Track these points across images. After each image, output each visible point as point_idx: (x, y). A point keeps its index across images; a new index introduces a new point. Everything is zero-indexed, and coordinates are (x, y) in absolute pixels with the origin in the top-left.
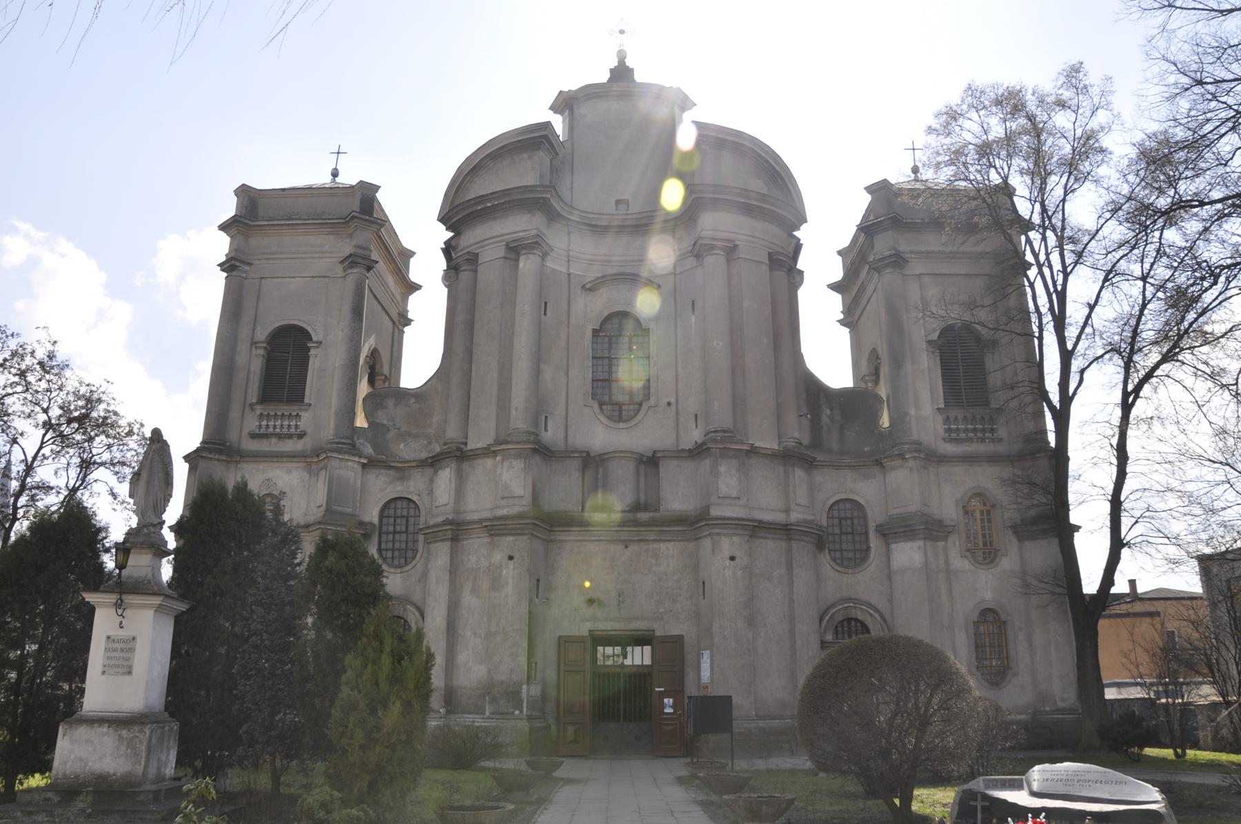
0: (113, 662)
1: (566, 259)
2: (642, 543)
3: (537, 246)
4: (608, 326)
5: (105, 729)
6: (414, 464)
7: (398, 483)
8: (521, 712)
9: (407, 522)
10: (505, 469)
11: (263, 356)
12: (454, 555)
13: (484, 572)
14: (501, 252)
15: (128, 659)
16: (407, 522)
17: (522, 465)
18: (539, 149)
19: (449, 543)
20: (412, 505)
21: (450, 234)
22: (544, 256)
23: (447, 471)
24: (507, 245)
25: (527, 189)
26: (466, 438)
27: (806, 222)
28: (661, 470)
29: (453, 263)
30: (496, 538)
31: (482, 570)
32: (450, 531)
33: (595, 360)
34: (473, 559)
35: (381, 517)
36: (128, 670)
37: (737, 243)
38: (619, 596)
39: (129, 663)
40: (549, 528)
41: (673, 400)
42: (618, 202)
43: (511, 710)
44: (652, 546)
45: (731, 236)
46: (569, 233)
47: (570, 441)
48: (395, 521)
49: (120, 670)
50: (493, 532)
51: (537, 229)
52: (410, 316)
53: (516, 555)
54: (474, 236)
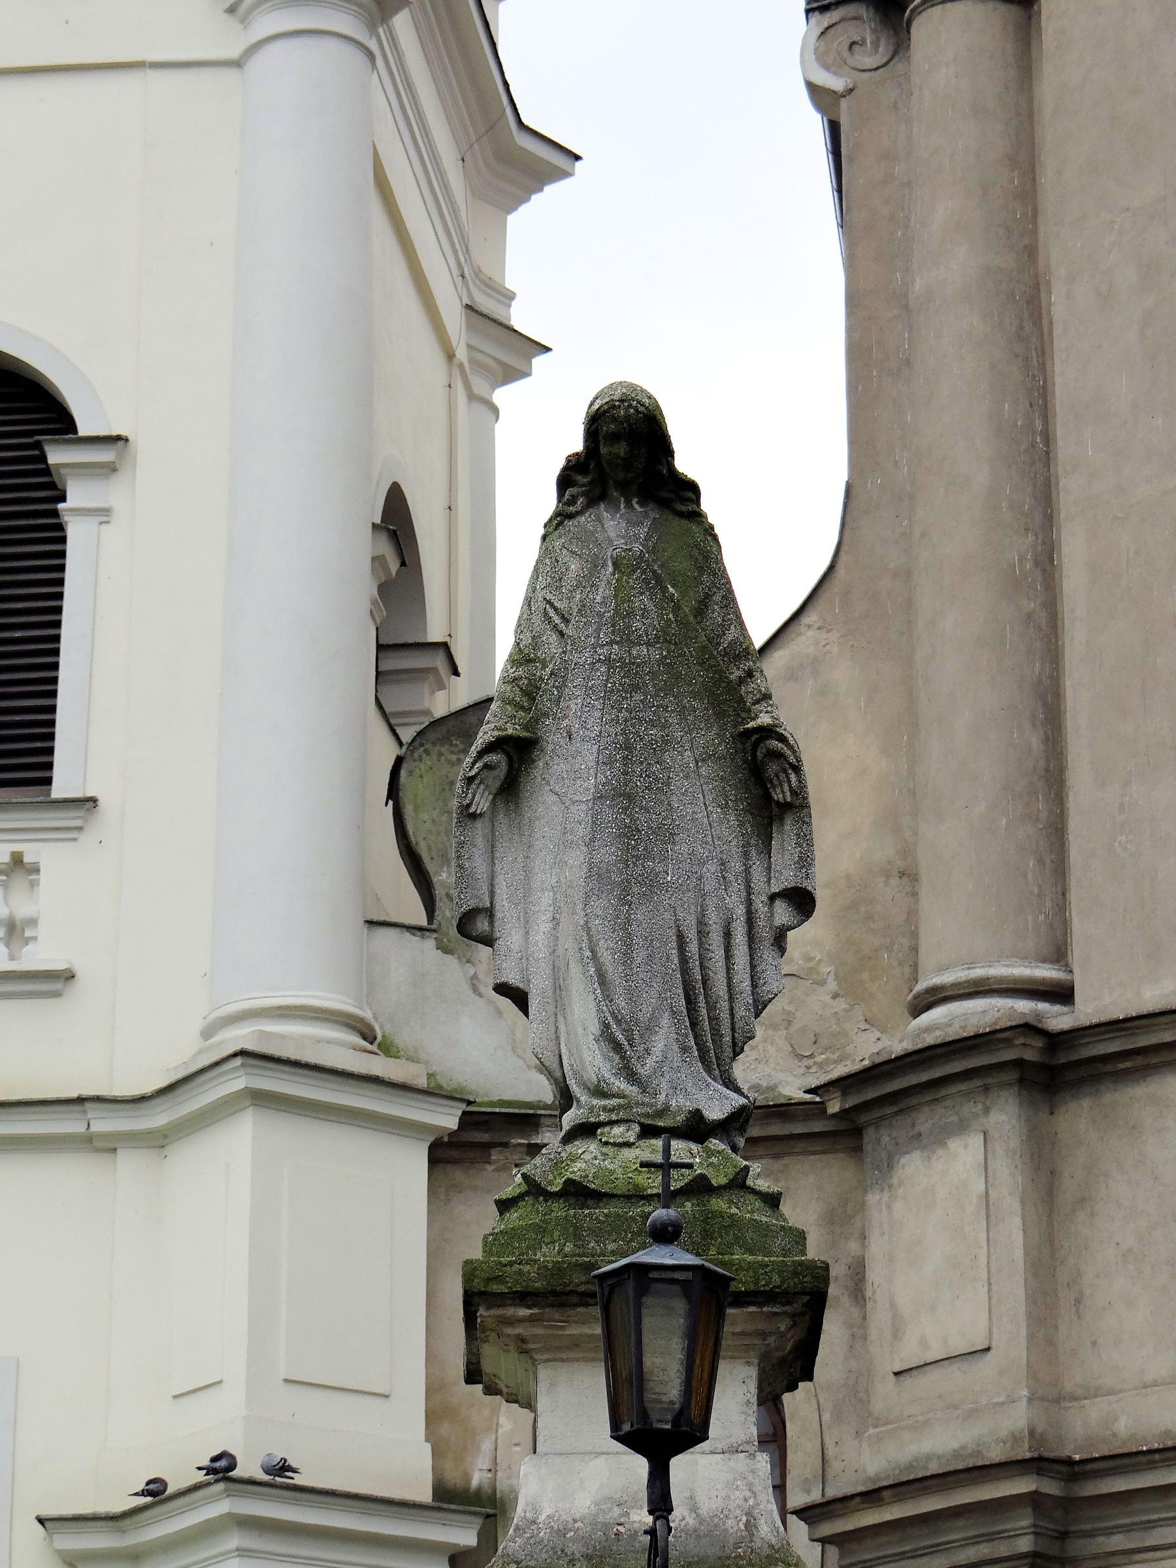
26: (1059, 954)
32: (1024, 1521)
52: (521, 319)
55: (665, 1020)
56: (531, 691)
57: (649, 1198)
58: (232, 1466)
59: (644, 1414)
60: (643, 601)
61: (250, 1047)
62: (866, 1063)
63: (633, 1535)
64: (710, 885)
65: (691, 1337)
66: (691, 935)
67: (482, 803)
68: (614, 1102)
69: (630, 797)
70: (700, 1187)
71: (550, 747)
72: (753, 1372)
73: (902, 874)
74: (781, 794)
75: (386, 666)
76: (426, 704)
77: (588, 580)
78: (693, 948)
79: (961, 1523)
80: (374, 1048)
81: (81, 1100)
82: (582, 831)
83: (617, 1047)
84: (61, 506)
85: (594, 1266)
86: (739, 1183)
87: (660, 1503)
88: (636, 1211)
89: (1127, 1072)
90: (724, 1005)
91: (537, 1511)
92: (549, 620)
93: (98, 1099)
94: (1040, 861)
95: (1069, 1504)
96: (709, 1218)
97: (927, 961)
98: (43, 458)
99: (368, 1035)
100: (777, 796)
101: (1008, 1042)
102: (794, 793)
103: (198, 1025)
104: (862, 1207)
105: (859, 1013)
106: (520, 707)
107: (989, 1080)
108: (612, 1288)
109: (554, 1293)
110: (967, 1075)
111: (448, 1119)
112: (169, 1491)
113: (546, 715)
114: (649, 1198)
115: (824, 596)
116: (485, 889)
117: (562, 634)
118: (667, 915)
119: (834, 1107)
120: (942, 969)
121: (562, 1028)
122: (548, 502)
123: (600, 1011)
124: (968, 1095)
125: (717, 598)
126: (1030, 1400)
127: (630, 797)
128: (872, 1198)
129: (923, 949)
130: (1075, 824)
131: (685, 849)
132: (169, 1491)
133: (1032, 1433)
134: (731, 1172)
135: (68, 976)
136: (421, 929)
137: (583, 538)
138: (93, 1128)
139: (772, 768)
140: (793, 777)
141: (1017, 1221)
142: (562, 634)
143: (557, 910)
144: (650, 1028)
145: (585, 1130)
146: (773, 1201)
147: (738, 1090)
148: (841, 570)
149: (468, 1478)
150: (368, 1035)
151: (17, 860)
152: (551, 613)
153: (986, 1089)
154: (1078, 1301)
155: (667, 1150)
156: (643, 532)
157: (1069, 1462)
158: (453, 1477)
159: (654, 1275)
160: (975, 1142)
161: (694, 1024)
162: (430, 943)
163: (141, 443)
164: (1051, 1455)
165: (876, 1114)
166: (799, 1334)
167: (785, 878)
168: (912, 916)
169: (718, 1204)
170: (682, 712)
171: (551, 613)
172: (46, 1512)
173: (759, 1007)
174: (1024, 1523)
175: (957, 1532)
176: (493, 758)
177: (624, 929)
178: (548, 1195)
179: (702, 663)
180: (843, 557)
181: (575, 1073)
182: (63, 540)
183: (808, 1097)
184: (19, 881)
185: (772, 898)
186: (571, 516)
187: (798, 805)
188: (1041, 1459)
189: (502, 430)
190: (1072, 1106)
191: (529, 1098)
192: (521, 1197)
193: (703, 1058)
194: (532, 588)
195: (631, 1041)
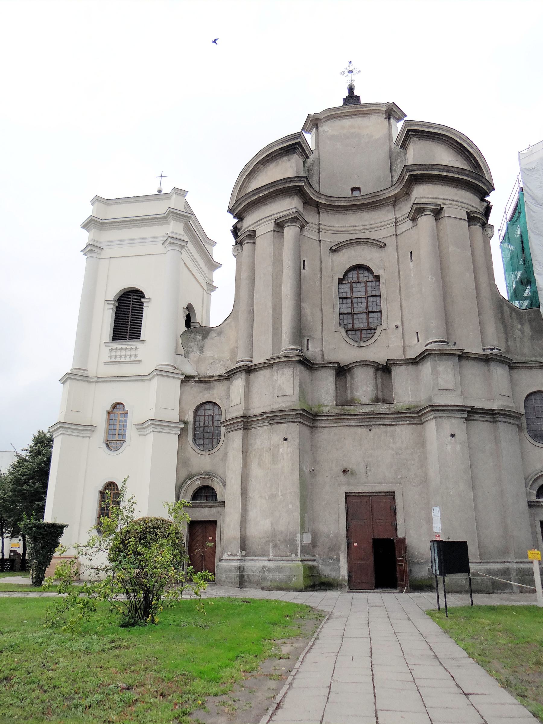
1: (318, 231)
2: (382, 427)
3: (295, 220)
4: (350, 276)
6: (217, 378)
7: (206, 392)
8: (296, 555)
9: (213, 418)
10: (279, 376)
12: (245, 440)
14: (271, 226)
16: (213, 418)
17: (291, 373)
18: (295, 153)
20: (216, 407)
21: (236, 221)
22: (302, 227)
23: (239, 380)
24: (275, 222)
25: (286, 180)
27: (494, 189)
28: (393, 373)
29: (239, 240)
30: (274, 426)
32: (242, 424)
33: (341, 300)
34: (258, 442)
35: (195, 415)
37: (442, 206)
38: (367, 466)
40: (311, 425)
41: (399, 323)
42: (353, 189)
43: (289, 554)
44: (390, 429)
45: (439, 201)
46: (319, 213)
47: (326, 357)
48: (204, 419)
50: (271, 422)
51: (295, 208)
54: (249, 222)
80: (176, 369)
81: (140, 375)
98: (141, 301)
99: (175, 368)
105: (232, 364)
111: (183, 377)
120: (239, 359)
150: (175, 368)
151: (136, 347)
158: (183, 419)
163: (152, 299)
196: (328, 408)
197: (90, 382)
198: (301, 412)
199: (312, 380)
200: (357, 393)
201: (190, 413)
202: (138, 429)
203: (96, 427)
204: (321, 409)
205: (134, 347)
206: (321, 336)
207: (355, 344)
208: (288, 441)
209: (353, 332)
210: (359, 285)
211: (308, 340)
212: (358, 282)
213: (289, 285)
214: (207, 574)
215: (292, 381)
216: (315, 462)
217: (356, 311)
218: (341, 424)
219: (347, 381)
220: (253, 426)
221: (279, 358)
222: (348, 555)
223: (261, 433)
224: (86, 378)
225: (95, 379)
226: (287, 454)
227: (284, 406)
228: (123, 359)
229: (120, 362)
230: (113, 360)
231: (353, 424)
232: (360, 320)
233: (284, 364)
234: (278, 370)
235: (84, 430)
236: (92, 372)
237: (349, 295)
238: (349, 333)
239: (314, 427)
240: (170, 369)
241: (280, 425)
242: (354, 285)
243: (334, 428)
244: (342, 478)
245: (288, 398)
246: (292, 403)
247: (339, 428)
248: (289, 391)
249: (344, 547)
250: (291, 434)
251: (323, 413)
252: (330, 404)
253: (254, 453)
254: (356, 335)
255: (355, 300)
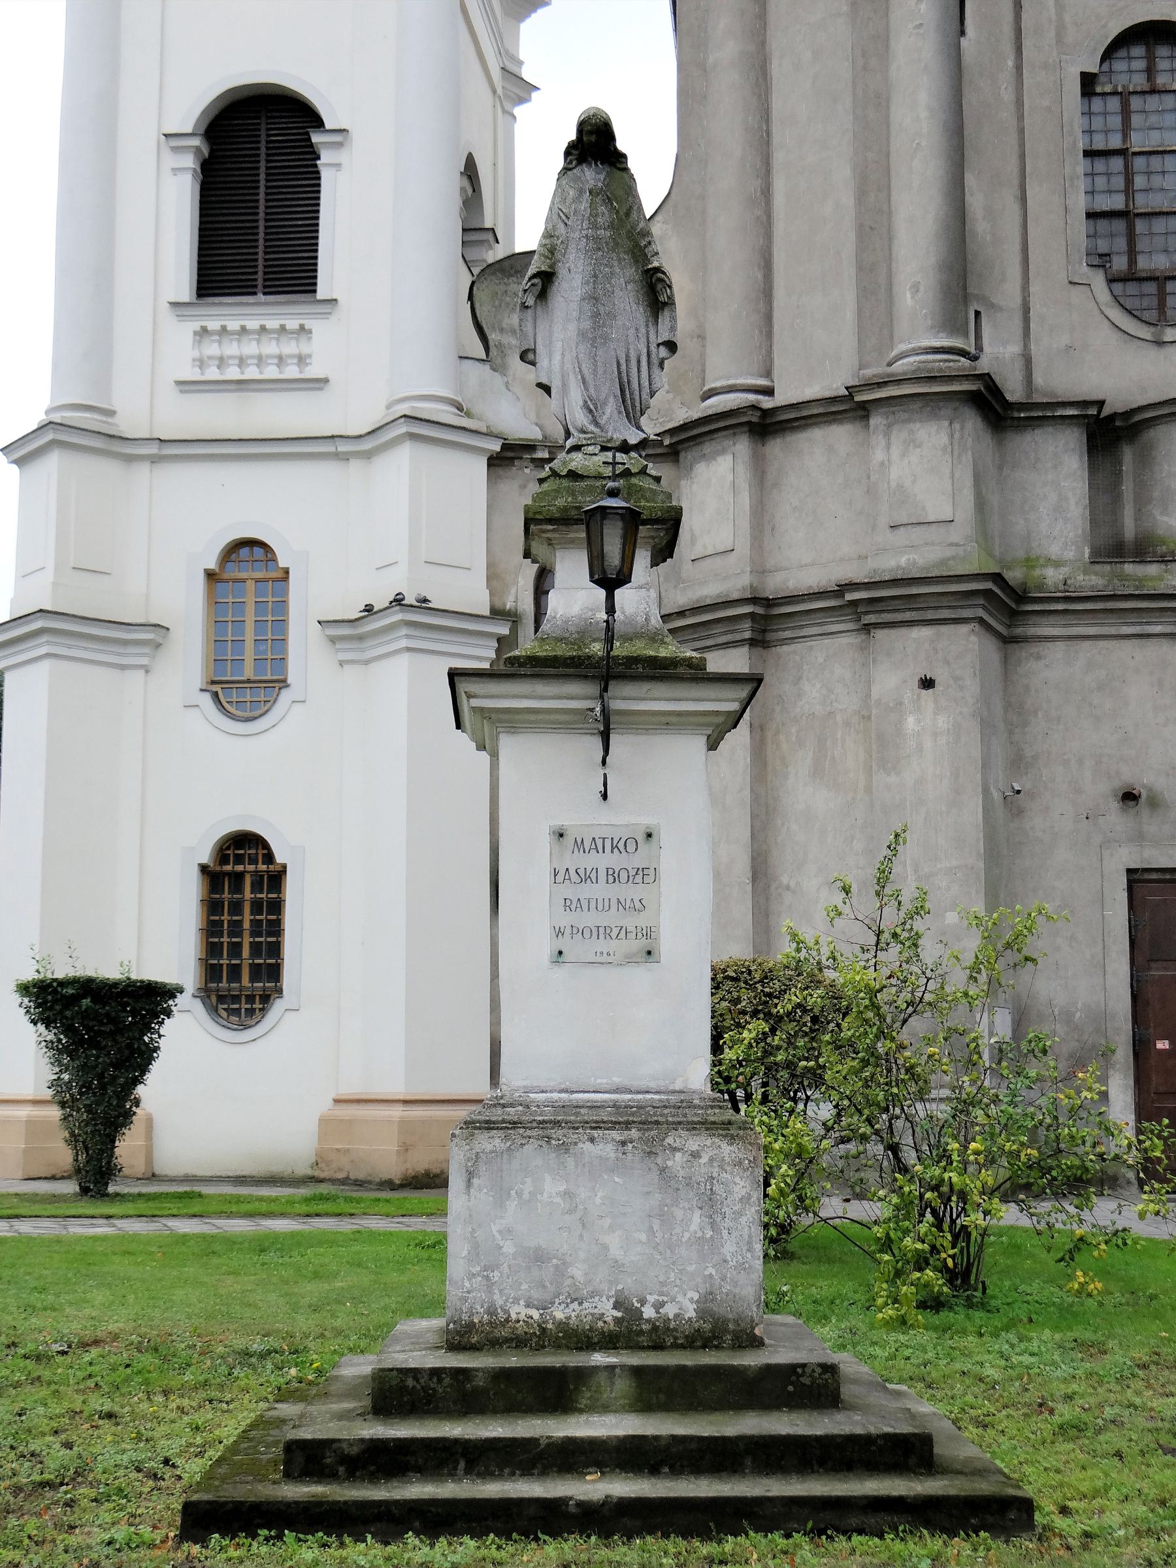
0: (589, 919)
5: (604, 1148)
10: (895, 451)
11: (198, 150)
13: (847, 724)
15: (640, 907)
17: (944, 439)
19: (745, 650)
26: (768, 374)
30: (880, 634)
31: (839, 718)
32: (747, 624)
36: (643, 943)
39: (642, 920)
47: (1039, 379)
49: (613, 945)
52: (527, 74)
53: (940, 675)
55: (611, 400)
56: (552, 251)
57: (604, 478)
58: (403, 599)
59: (604, 571)
60: (602, 209)
61: (408, 413)
62: (681, 422)
63: (598, 623)
64: (631, 339)
65: (625, 538)
66: (623, 362)
67: (530, 301)
68: (589, 436)
69: (596, 299)
70: (627, 473)
71: (560, 276)
72: (649, 554)
73: (699, 337)
74: (663, 298)
75: (466, 239)
76: (484, 257)
77: (577, 200)
78: (624, 367)
79: (720, 625)
81: (333, 437)
82: (575, 314)
83: (590, 411)
84: (318, 162)
85: (581, 507)
86: (643, 472)
87: (611, 609)
88: (598, 484)
89: (798, 427)
90: (637, 393)
91: (556, 613)
92: (560, 217)
93: (341, 436)
94: (761, 331)
95: (766, 617)
96: (630, 486)
97: (709, 375)
98: (309, 139)
99: (460, 408)
100: (661, 299)
101: (744, 413)
102: (668, 297)
103: (384, 403)
104: (678, 487)
106: (547, 257)
107: (736, 430)
108: (590, 517)
109: (563, 519)
110: (726, 428)
111: (496, 447)
112: (375, 610)
113: (559, 261)
114: (604, 478)
115: (665, 208)
116: (532, 340)
117: (566, 224)
118: (613, 353)
119: (667, 442)
120: (716, 380)
121: (566, 403)
122: (560, 163)
123: (583, 395)
124: (726, 437)
125: (635, 208)
126: (751, 572)
127: (596, 299)
128: (683, 483)
129: (707, 372)
130: (776, 314)
131: (620, 323)
132: (375, 610)
133: (751, 586)
134: (640, 467)
135: (326, 381)
136: (483, 360)
137: (577, 179)
138: (339, 450)
139: (659, 286)
140: (668, 290)
141: (747, 493)
142: (566, 224)
143: (564, 349)
144: (605, 403)
145: (577, 448)
146: (658, 479)
147: (643, 431)
148: (673, 195)
149: (505, 605)
150: (460, 408)
151: (302, 327)
152: (562, 215)
153: (734, 434)
154: (773, 529)
155: (614, 457)
156: (602, 177)
157: (767, 599)
158: (498, 605)
159: (608, 511)
160: (729, 458)
161: (624, 401)
162: (487, 367)
163: (355, 133)
164: (760, 596)
165: (686, 445)
166: (668, 538)
167: (665, 336)
168: (703, 356)
169: (634, 480)
170: (619, 260)
171: (562, 215)
172: (322, 619)
173: (652, 394)
174: (747, 626)
175: (717, 630)
176: (535, 281)
177: (594, 358)
178: (560, 476)
179: (628, 238)
180: (674, 189)
181: (573, 423)
182: (319, 178)
183: (655, 437)
184: (303, 338)
185: (658, 345)
186: (570, 169)
187: (670, 303)
188: (755, 598)
189: (518, 127)
190: (773, 442)
191: (532, 437)
192: (548, 477)
193: (628, 416)
194: (553, 202)
195: (596, 408)
196: (1064, 572)
197: (130, 459)
198: (988, 585)
199: (1000, 468)
200: (1165, 519)
201: (521, 582)
202: (333, 640)
203: (168, 629)
204: (1037, 572)
205: (292, 324)
206: (1019, 301)
207: (1145, 332)
208: (939, 687)
209: (1132, 288)
210: (1153, 102)
211: (978, 314)
212: (1153, 91)
213: (923, 97)
214: (1148, 1138)
215: (947, 471)
216: (1018, 762)
217: (1142, 203)
218: (1113, 631)
219: (1121, 471)
220: (788, 634)
221: (899, 382)
222: (1137, 1081)
223: (821, 660)
224: (115, 442)
225: (153, 449)
226: (935, 735)
227: (921, 561)
228: (252, 373)
229: (241, 385)
230: (213, 373)
231: (1158, 629)
232: (1159, 241)
233: (916, 405)
234: (889, 426)
235: (126, 643)
236: (129, 422)
237: (1115, 142)
238: (1118, 287)
239: (1012, 637)
240: (447, 415)
241: (903, 631)
242: (1136, 103)
243: (1086, 644)
244: (1115, 818)
245: (933, 533)
246: (949, 552)
247: (1102, 644)
248: (938, 506)
249: (1123, 1053)
250: (948, 663)
251: (1041, 587)
252: (1070, 554)
253: (794, 730)
254: (1142, 296)
255: (1139, 163)
